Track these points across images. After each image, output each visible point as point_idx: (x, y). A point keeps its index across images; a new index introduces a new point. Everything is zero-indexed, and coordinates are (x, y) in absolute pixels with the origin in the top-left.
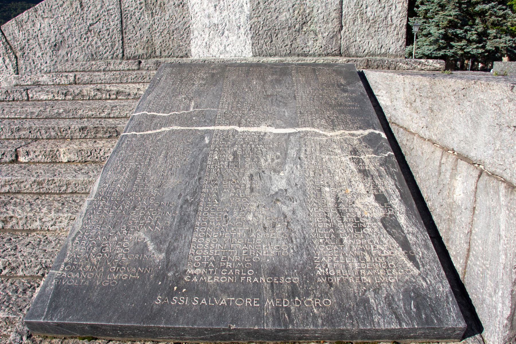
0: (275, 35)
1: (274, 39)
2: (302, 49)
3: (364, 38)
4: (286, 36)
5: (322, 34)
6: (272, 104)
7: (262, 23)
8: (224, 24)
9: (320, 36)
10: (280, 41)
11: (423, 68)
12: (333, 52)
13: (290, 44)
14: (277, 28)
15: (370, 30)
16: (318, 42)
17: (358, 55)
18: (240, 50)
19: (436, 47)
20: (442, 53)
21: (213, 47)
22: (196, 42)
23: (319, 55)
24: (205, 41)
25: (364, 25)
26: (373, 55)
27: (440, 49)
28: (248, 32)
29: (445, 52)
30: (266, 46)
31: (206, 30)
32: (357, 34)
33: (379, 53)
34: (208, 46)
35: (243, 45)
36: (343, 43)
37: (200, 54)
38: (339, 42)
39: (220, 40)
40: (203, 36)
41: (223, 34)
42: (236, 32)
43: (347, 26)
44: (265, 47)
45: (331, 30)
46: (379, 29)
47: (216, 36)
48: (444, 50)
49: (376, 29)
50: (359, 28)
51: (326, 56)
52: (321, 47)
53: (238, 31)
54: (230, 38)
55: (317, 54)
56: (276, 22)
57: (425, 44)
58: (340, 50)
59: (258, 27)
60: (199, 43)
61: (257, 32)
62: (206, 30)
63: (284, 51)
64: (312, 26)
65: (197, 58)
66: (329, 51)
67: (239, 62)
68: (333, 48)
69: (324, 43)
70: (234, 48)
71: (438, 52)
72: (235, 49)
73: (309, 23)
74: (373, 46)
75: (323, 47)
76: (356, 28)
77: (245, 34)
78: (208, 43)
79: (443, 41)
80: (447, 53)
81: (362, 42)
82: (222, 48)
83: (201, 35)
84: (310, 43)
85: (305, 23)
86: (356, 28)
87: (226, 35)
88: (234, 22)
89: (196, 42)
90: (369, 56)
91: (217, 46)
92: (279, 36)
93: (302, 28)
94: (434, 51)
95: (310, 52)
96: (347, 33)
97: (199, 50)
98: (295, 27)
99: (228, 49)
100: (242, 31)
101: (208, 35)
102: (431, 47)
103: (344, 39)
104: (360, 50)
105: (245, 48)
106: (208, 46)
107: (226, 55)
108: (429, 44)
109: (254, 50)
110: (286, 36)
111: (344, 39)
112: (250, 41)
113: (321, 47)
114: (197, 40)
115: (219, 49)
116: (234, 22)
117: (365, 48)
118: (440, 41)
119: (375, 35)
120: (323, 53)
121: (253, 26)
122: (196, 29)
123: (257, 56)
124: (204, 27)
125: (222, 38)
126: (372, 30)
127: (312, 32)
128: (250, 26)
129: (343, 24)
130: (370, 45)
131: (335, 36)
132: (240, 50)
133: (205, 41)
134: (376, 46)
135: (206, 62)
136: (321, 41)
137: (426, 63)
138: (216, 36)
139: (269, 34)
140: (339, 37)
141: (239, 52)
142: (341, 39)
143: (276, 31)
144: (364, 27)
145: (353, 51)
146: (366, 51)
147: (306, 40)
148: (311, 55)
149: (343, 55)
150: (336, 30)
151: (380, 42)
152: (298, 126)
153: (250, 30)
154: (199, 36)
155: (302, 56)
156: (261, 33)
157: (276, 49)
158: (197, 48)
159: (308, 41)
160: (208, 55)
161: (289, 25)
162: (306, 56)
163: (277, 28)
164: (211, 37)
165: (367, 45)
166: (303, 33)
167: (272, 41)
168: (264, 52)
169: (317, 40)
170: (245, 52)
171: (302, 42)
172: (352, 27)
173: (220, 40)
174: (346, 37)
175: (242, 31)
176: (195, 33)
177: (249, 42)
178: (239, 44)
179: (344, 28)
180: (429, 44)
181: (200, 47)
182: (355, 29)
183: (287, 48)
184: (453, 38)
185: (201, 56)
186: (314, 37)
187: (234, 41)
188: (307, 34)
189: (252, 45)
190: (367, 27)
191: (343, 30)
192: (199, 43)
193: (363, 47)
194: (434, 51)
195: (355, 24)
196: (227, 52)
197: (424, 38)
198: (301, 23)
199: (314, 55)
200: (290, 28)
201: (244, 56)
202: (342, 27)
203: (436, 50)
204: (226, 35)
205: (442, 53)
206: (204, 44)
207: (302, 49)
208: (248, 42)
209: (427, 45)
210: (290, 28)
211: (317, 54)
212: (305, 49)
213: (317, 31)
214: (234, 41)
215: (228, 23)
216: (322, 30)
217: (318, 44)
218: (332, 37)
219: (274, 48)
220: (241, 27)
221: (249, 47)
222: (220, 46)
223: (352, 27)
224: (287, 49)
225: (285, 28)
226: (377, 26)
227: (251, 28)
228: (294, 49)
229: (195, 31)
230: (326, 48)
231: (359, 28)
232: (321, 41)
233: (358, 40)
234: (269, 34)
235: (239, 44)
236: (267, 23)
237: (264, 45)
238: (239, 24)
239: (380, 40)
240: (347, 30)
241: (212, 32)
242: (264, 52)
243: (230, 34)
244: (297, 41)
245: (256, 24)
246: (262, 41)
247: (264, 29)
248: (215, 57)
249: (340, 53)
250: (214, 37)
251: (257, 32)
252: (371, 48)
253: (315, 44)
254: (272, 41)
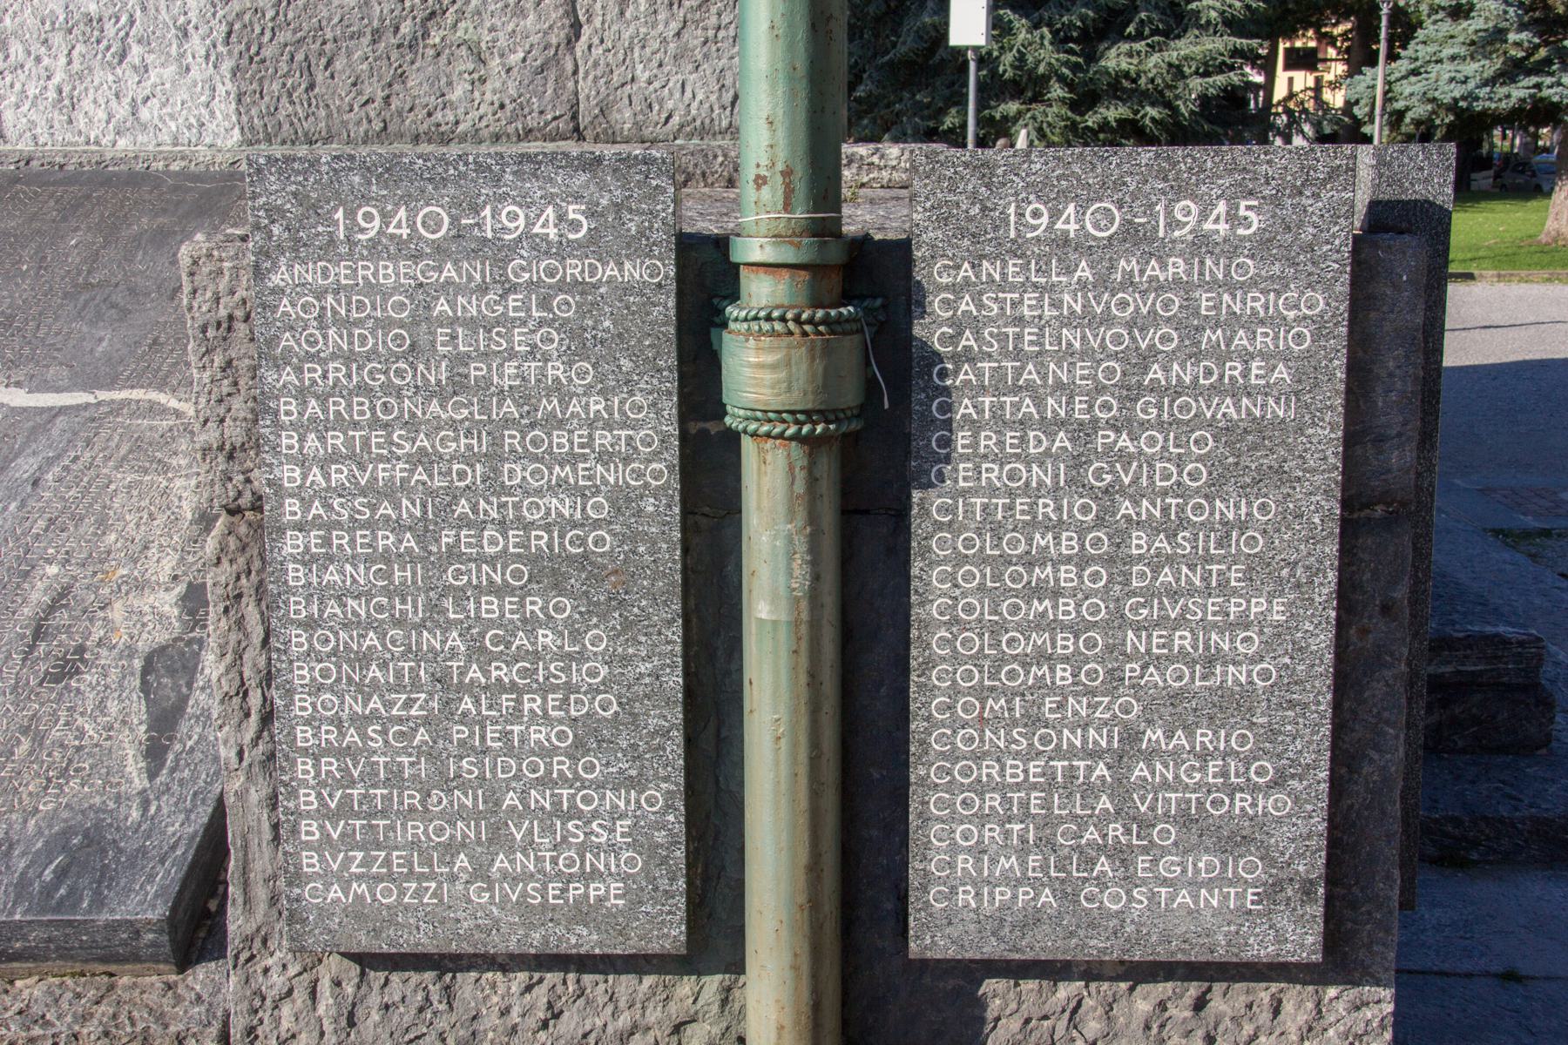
0: (324, 61)
1: (319, 78)
2: (430, 115)
3: (666, 69)
4: (365, 66)
5: (502, 56)
6: (80, 316)
7: (270, 14)
8: (124, 20)
9: (495, 63)
10: (342, 84)
11: (865, 180)
12: (547, 124)
13: (380, 94)
14: (329, 36)
15: (686, 35)
16: (489, 86)
17: (647, 132)
18: (193, 121)
19: (1492, 66)
20: (1523, 93)
21: (87, 104)
22: (18, 86)
23: (497, 138)
24: (56, 80)
25: (661, 17)
26: (703, 132)
27: (1513, 71)
28: (220, 48)
29: (1538, 86)
30: (292, 103)
31: (57, 39)
32: (636, 54)
33: (725, 123)
34: (67, 102)
35: (203, 99)
36: (585, 87)
37: (39, 130)
38: (570, 84)
39: (111, 78)
40: (46, 61)
41: (123, 55)
42: (174, 50)
43: (597, 22)
44: (285, 108)
45: (535, 39)
46: (721, 34)
47: (96, 64)
48: (1534, 80)
49: (711, 33)
50: (643, 30)
51: (519, 140)
52: (502, 106)
53: (180, 46)
54: (153, 74)
55: (485, 133)
56: (325, 13)
57: (1447, 52)
58: (574, 117)
59: (258, 30)
60: (32, 91)
61: (253, 50)
62: (57, 39)
63: (359, 123)
64: (462, 25)
65: (25, 146)
66: (532, 122)
67: (160, 165)
68: (546, 106)
69: (513, 92)
70: (168, 110)
71: (1502, 91)
72: (172, 116)
73: (450, 16)
74: (700, 97)
75: (509, 107)
76: (631, 30)
77: (207, 57)
78: (66, 89)
79: (1524, 36)
80: (1546, 93)
81: (657, 85)
82: (122, 111)
83: (38, 60)
84: (458, 92)
85: (433, 14)
86: (631, 30)
87: (137, 61)
88: (164, 12)
89: (18, 86)
90: (690, 136)
91: (102, 101)
92: (338, 65)
93: (426, 35)
94: (1485, 83)
95: (461, 128)
96: (598, 51)
97: (33, 116)
98: (397, 29)
99: (144, 114)
100: (196, 44)
101: (63, 60)
102: (1470, 68)
103: (587, 73)
104: (654, 116)
105: (212, 113)
106: (68, 103)
107: (140, 138)
108: (1463, 51)
109: (245, 119)
110: (365, 66)
111: (587, 73)
112: (229, 86)
113: (502, 106)
114: (22, 77)
115: (110, 117)
116: (164, 12)
117: (670, 105)
118: (1512, 37)
119: (706, 56)
120: (511, 129)
121: (237, 27)
122: (14, 33)
123: (258, 142)
124: (48, 26)
125: (119, 71)
126: (694, 37)
127: (464, 51)
128: (224, 28)
129: (582, 19)
130: (688, 94)
131: (550, 63)
132: (193, 121)
133: (56, 80)
134: (713, 98)
135: (34, 163)
136: (498, 85)
137: (875, 159)
138: (96, 64)
139: (300, 57)
140: (569, 67)
141: (189, 127)
142: (575, 72)
143: (327, 47)
144: (661, 27)
145: (624, 117)
146: (676, 120)
147: (444, 80)
148: (463, 139)
149: (589, 134)
150: (554, 41)
151: (728, 82)
152: (111, 385)
153: (227, 42)
154: (29, 64)
155: (429, 141)
156: (267, 52)
157: (329, 116)
158: (25, 108)
159: (450, 84)
160: (69, 136)
161: (375, 24)
162: (445, 140)
163: (329, 36)
164: (76, 66)
165: (677, 95)
166: (431, 52)
167: (311, 86)
168: (286, 127)
169: (483, 81)
170: (212, 127)
171: (426, 87)
172: (615, 28)
173: (111, 78)
174: (596, 64)
175: (196, 44)
176: (12, 51)
177: (226, 87)
178: (186, 96)
179: (586, 31)
180: (1463, 51)
181: (34, 104)
182: (626, 35)
183: (371, 110)
184: (1314, 51)
185: (41, 140)
186: (471, 66)
187: (168, 86)
188: (443, 59)
189: (239, 101)
190: (674, 26)
191: (583, 39)
192: (32, 91)
193: (661, 102)
194: (1485, 83)
195: (628, 15)
196: (144, 127)
197: (1447, 27)
198: (420, 16)
199: (475, 137)
200: (377, 36)
201: (208, 141)
202: (576, 27)
203: (1490, 82)
204: (137, 61)
205: (1519, 91)
206: (51, 94)
207: (430, 115)
208: (221, 90)
209: (1453, 58)
210: (377, 36)
211: (485, 133)
212: (438, 116)
213: (483, 45)
214: (168, 86)
215: (138, 13)
216: (503, 42)
217: (488, 97)
218: (542, 69)
219: (322, 113)
220: (190, 28)
221: (225, 109)
222: (114, 103)
223: (615, 28)
224: (372, 114)
225: (360, 34)
226: (714, 20)
227: (229, 34)
228: (400, 114)
229: (12, 40)
230: (521, 111)
231: (643, 30)
232: (498, 85)
233: (643, 76)
234: (300, 57)
235: (186, 96)
236: (291, 15)
237: (284, 100)
238: (182, 20)
239: (728, 74)
240: (596, 41)
241: (80, 48)
242: (286, 127)
243: (150, 58)
244: (410, 84)
245: (247, 17)
246: (276, 86)
247: (282, 37)
248: (97, 143)
249: (577, 129)
250: (90, 69)
251: (253, 50)
252: (695, 105)
253: (477, 94)
254: (311, 86)
